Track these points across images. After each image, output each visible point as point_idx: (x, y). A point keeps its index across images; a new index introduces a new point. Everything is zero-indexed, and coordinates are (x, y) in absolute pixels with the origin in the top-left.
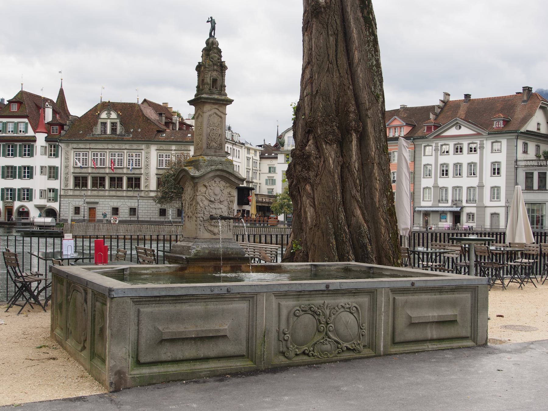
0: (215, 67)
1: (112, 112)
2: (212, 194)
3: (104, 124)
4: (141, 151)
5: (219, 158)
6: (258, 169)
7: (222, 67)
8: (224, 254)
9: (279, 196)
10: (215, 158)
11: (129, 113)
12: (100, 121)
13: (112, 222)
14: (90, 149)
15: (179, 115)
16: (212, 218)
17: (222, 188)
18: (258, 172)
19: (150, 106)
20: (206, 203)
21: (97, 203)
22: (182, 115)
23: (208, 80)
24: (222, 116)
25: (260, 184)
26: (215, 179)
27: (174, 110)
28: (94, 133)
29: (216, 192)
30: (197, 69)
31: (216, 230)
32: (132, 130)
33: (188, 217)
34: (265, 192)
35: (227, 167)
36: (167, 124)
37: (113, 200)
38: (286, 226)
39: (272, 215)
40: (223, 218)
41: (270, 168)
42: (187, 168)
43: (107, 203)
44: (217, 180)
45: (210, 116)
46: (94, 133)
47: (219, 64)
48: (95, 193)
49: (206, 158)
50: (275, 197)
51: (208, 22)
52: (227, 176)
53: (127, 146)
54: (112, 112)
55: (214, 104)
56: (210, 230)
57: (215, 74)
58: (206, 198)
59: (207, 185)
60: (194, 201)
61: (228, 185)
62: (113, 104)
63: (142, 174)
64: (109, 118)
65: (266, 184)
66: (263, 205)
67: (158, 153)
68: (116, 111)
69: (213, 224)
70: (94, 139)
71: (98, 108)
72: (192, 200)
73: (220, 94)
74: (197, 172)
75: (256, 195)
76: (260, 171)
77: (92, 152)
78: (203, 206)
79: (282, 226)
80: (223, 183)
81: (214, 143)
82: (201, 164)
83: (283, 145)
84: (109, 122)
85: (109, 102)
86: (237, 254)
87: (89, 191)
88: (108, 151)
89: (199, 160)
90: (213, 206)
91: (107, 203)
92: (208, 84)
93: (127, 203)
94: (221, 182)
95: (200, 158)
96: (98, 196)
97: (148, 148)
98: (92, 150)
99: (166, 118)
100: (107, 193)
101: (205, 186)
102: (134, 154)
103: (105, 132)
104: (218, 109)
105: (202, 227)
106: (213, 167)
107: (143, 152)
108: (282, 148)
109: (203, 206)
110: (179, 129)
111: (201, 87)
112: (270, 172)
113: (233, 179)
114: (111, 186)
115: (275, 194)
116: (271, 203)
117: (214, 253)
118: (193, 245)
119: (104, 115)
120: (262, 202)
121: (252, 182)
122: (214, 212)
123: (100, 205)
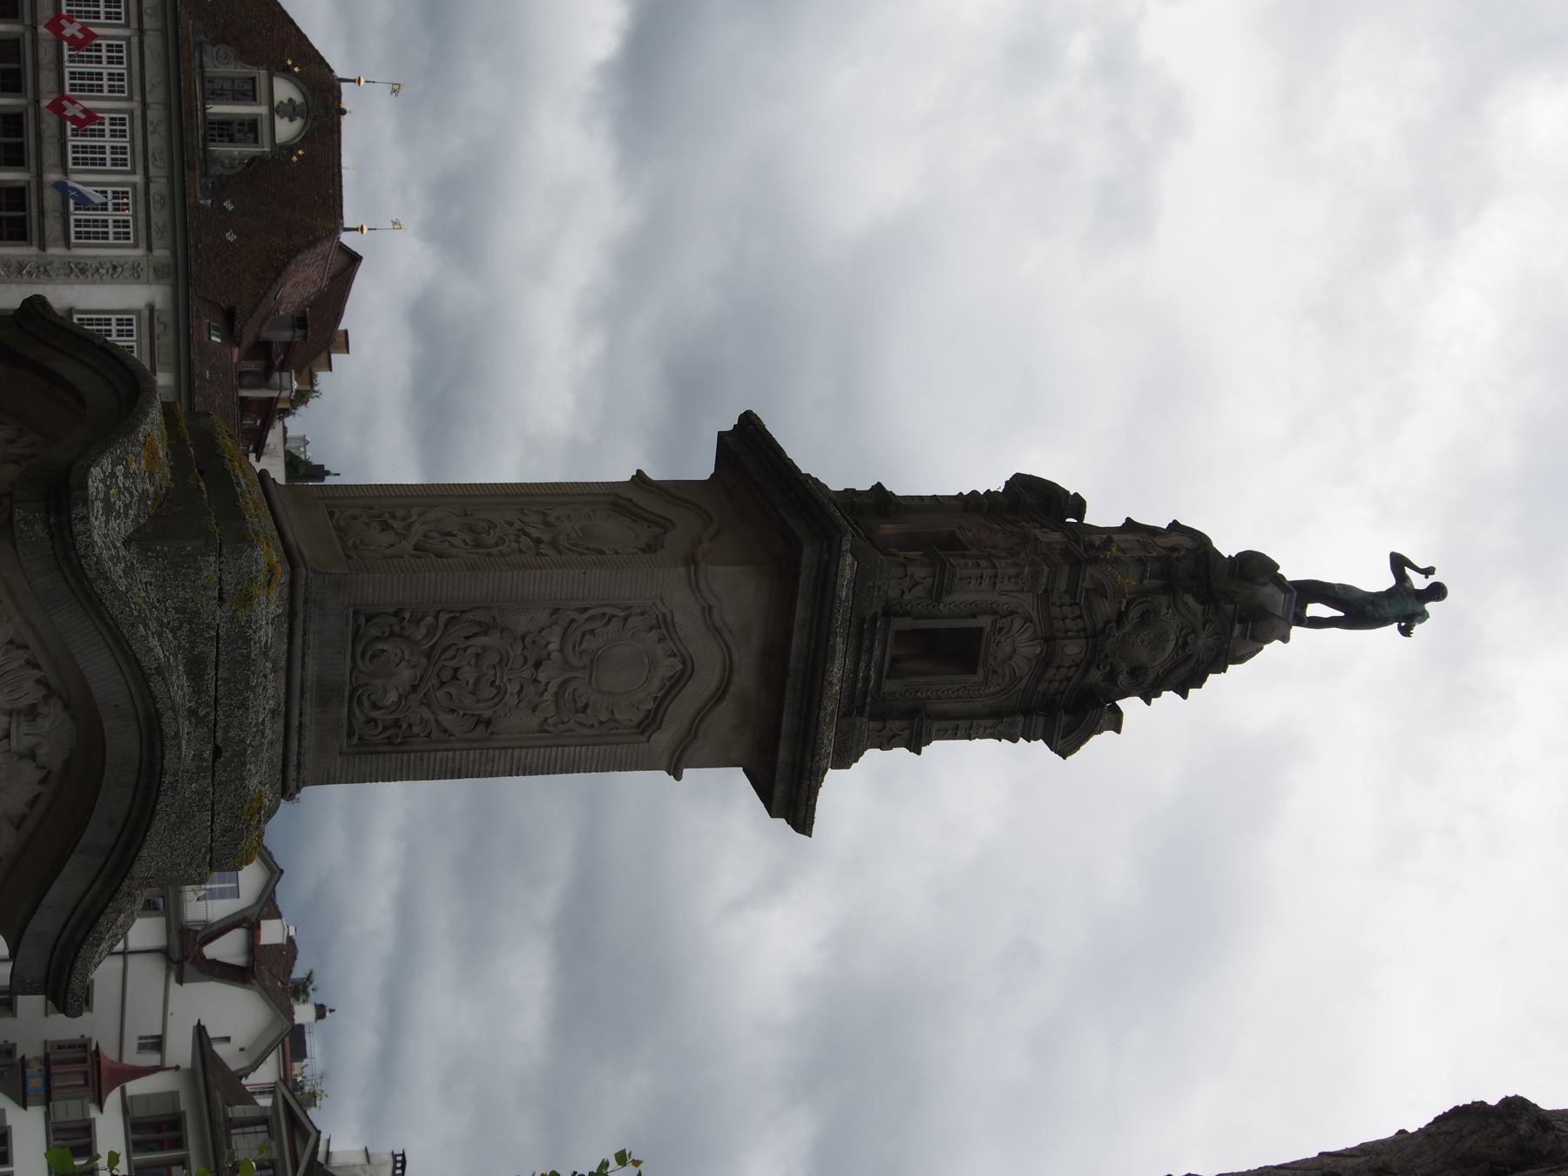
0: (1073, 649)
1: (298, 123)
3: (247, 93)
4: (143, 244)
5: (273, 731)
7: (1068, 713)
10: (268, 692)
11: (303, 189)
12: (261, 74)
14: (141, 31)
15: (302, 398)
19: (333, 278)
22: (302, 409)
23: (970, 593)
24: (660, 737)
27: (322, 377)
28: (210, 50)
30: (1023, 486)
32: (229, 205)
36: (262, 349)
42: (153, 424)
44: (52, 733)
45: (664, 625)
46: (210, 50)
47: (1096, 676)
49: (268, 606)
51: (1399, 563)
53: (159, 186)
54: (298, 123)
55: (774, 656)
57: (1018, 648)
63: (42, 247)
67: (138, 312)
68: (306, 139)
73: (854, 705)
74: (121, 528)
81: (406, 674)
82: (210, 567)
84: (261, 110)
85: (344, 112)
88: (136, 105)
89: (244, 539)
92: (938, 592)
94: (30, 774)
95: (266, 554)
97: (159, 273)
98: (135, 40)
99: (288, 347)
102: (127, 215)
103: (219, 96)
104: (720, 695)
106: (179, 688)
107: (139, 252)
110: (242, 399)
111: (887, 529)
113: (66, 889)
119: (284, 90)
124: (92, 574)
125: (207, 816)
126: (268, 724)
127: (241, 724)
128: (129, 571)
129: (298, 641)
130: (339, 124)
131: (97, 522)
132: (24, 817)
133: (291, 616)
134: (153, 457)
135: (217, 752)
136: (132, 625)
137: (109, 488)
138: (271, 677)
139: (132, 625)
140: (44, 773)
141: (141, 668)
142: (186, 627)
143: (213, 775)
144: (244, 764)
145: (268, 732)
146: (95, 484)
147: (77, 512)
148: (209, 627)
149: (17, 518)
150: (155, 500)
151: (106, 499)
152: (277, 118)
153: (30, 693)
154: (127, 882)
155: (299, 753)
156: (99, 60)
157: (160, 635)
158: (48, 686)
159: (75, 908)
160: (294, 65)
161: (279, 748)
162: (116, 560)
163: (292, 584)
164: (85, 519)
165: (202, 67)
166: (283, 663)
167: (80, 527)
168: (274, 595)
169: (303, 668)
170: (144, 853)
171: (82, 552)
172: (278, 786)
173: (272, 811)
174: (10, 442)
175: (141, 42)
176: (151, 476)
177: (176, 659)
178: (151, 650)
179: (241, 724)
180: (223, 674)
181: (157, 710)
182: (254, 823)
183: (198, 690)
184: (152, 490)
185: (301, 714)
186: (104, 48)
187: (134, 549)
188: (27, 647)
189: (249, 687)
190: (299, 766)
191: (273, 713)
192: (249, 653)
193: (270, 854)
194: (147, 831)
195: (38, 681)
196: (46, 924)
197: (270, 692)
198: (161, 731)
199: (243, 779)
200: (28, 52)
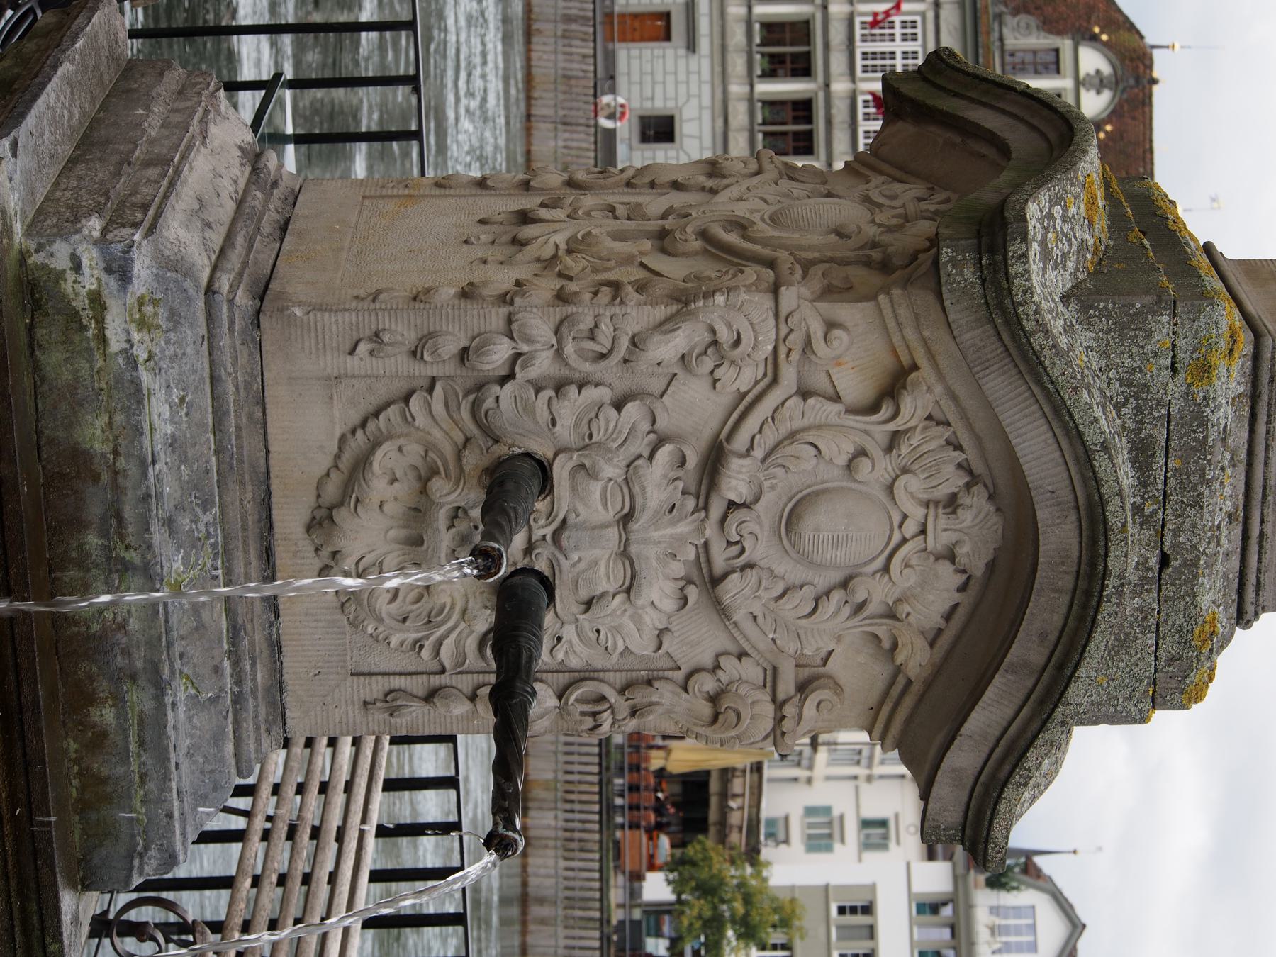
1: (1106, 95)
2: (804, 467)
5: (1230, 538)
6: (878, 770)
8: (77, 647)
9: (758, 875)
12: (1066, 44)
13: (606, 99)
16: (513, 482)
17: (877, 592)
18: (861, 771)
20: (695, 407)
21: (692, 46)
25: (809, 781)
26: (976, 508)
28: (1010, 21)
29: (822, 522)
31: (369, 531)
33: (525, 218)
34: (770, 807)
35: (1123, 643)
37: (706, 116)
38: (617, 916)
39: (664, 841)
40: (519, 606)
41: (883, 823)
43: (694, 89)
44: (974, 529)
46: (1010, 21)
48: (737, 36)
49: (1229, 381)
50: (752, 854)
52: (1029, 648)
54: (1106, 95)
56: (362, 463)
58: (744, 405)
59: (913, 406)
60: (709, 269)
61: (916, 658)
62: (1145, 103)
64: (1078, 83)
65: (810, 811)
66: (714, 801)
68: (1115, 113)
69: (446, 494)
70: (983, 20)
71: (1124, 36)
72: (713, 246)
74: (1059, 281)
75: (758, 768)
76: (869, 779)
77: (923, 15)
78: (645, 375)
79: (616, 895)
80: (932, 595)
83: (997, 882)
85: (1154, 81)
86: (98, 794)
87: (743, 11)
90: (658, 483)
91: (694, 89)
93: (694, 102)
94: (948, 577)
96: (724, 48)
98: (930, 15)
100: (737, 89)
101: (892, 389)
105: (396, 368)
108: (982, 878)
109: (645, 375)
112: (866, 824)
113: (988, 716)
114: (772, 104)
115: (766, 853)
116: (722, 838)
117: (79, 525)
118: (172, 266)
119: (1092, 61)
120: (725, 795)
121: (814, 744)
122: (585, 501)
123: (682, 63)
124: (1030, 326)
125: (1150, 638)
126: (1224, 529)
127: (1194, 526)
128: (1069, 328)
129: (1261, 429)
130: (1150, 96)
131: (1035, 266)
132: (940, 631)
133: (1254, 397)
134: (1092, 202)
135: (1165, 561)
136: (1075, 389)
137: (1046, 230)
138: (1229, 471)
139: (1075, 389)
140: (965, 577)
141: (1083, 444)
142: (1132, 403)
143: (1159, 590)
144: (1196, 577)
145: (1224, 541)
146: (1033, 210)
147: (1014, 248)
148: (1159, 403)
149: (944, 258)
150: (1095, 254)
151: (1043, 244)
152: (1083, 92)
153: (952, 481)
154: (1061, 708)
155: (1259, 571)
156: (892, 38)
157: (1104, 408)
158: (970, 472)
159: (999, 740)
160: (1102, 32)
161: (1235, 562)
162: (1057, 316)
163: (1256, 357)
164: (1024, 257)
165: (1001, 39)
166: (1243, 455)
167: (1016, 268)
168: (1235, 369)
169: (1266, 464)
170: (1082, 672)
171: (1018, 299)
172: (1234, 609)
173: (1226, 640)
174: (920, 200)
175: (937, 17)
176: (1091, 225)
177: (1120, 440)
178: (1096, 420)
179: (1194, 526)
180: (1174, 463)
181: (1101, 496)
182: (1206, 651)
183: (1144, 483)
184: (1091, 242)
185: (1262, 522)
186: (898, 25)
187: (1073, 306)
188: (949, 424)
189: (1205, 481)
190: (1258, 586)
191: (1231, 517)
192: (1206, 438)
193: (1071, 906)
194: (1085, 646)
195: (959, 466)
196: (964, 758)
197: (1228, 490)
198: (1105, 521)
199: (1194, 595)
200: (729, 258)
